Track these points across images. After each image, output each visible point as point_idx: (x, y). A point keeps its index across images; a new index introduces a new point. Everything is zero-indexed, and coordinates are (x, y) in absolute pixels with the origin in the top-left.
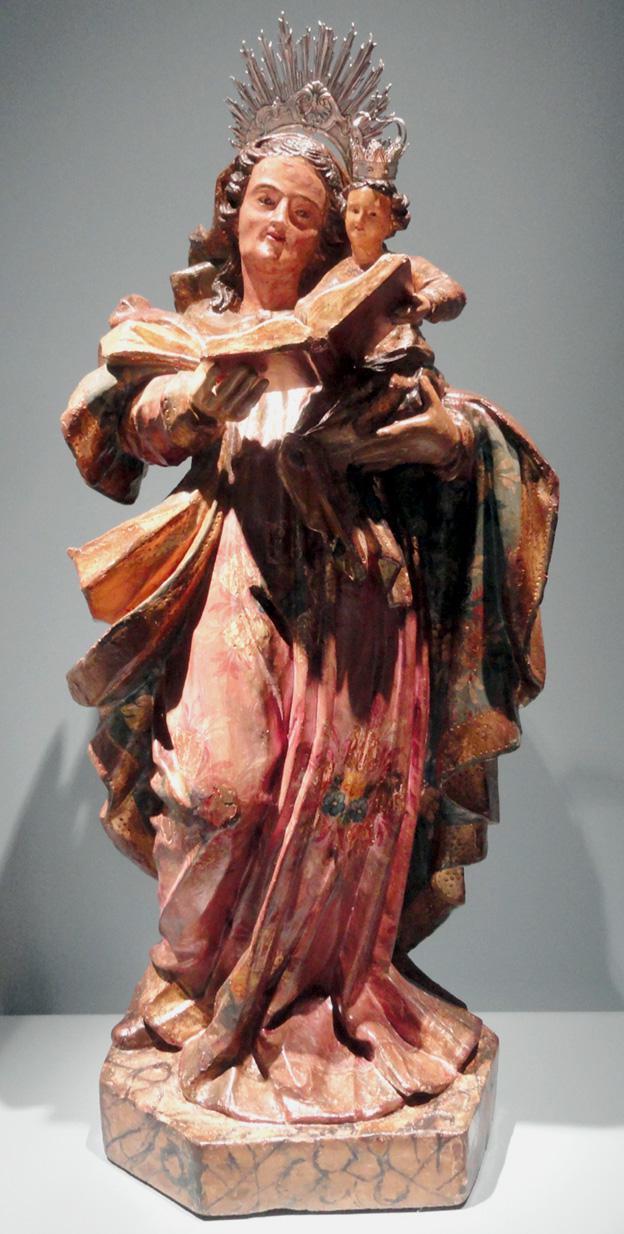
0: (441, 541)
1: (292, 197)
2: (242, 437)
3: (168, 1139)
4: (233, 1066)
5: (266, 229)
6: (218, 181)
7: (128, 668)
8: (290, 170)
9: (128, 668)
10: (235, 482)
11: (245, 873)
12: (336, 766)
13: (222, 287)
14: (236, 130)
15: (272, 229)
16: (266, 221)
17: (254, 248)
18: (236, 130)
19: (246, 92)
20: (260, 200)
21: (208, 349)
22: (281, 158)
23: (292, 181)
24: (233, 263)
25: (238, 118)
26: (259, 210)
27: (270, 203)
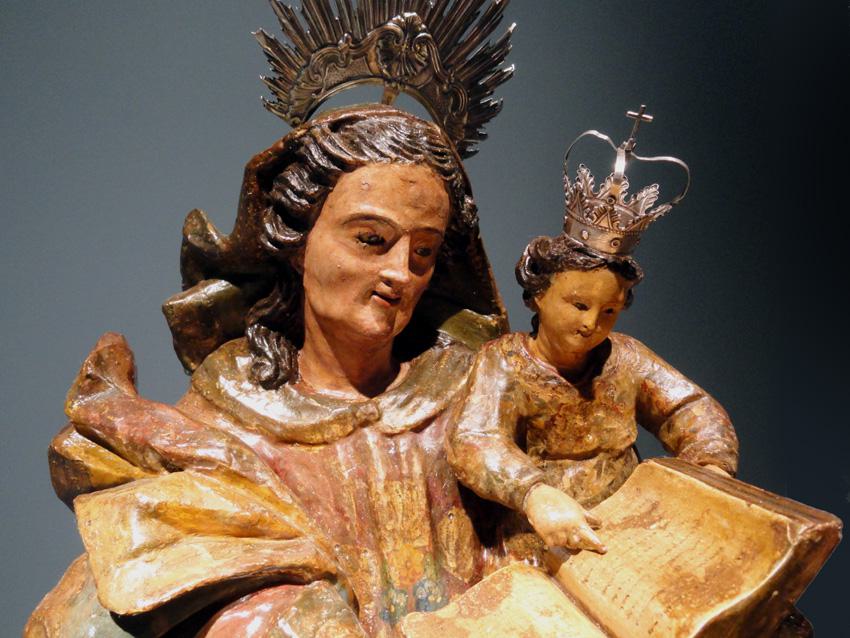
0: (192, 364)
1: (415, 234)
2: (497, 428)
3: (404, 614)
4: (440, 324)
5: (374, 284)
6: (248, 172)
7: (628, 212)
8: (413, 189)
9: (628, 212)
10: (648, 184)
11: (463, 52)
12: (333, 80)
13: (267, 336)
14: (273, 81)
15: (385, 288)
16: (372, 273)
17: (350, 315)
18: (273, 81)
19: (292, 21)
20: (360, 238)
21: (757, 533)
22: (396, 167)
23: (416, 208)
24: (284, 300)
25: (277, 62)
26: (360, 256)
27: (377, 242)
